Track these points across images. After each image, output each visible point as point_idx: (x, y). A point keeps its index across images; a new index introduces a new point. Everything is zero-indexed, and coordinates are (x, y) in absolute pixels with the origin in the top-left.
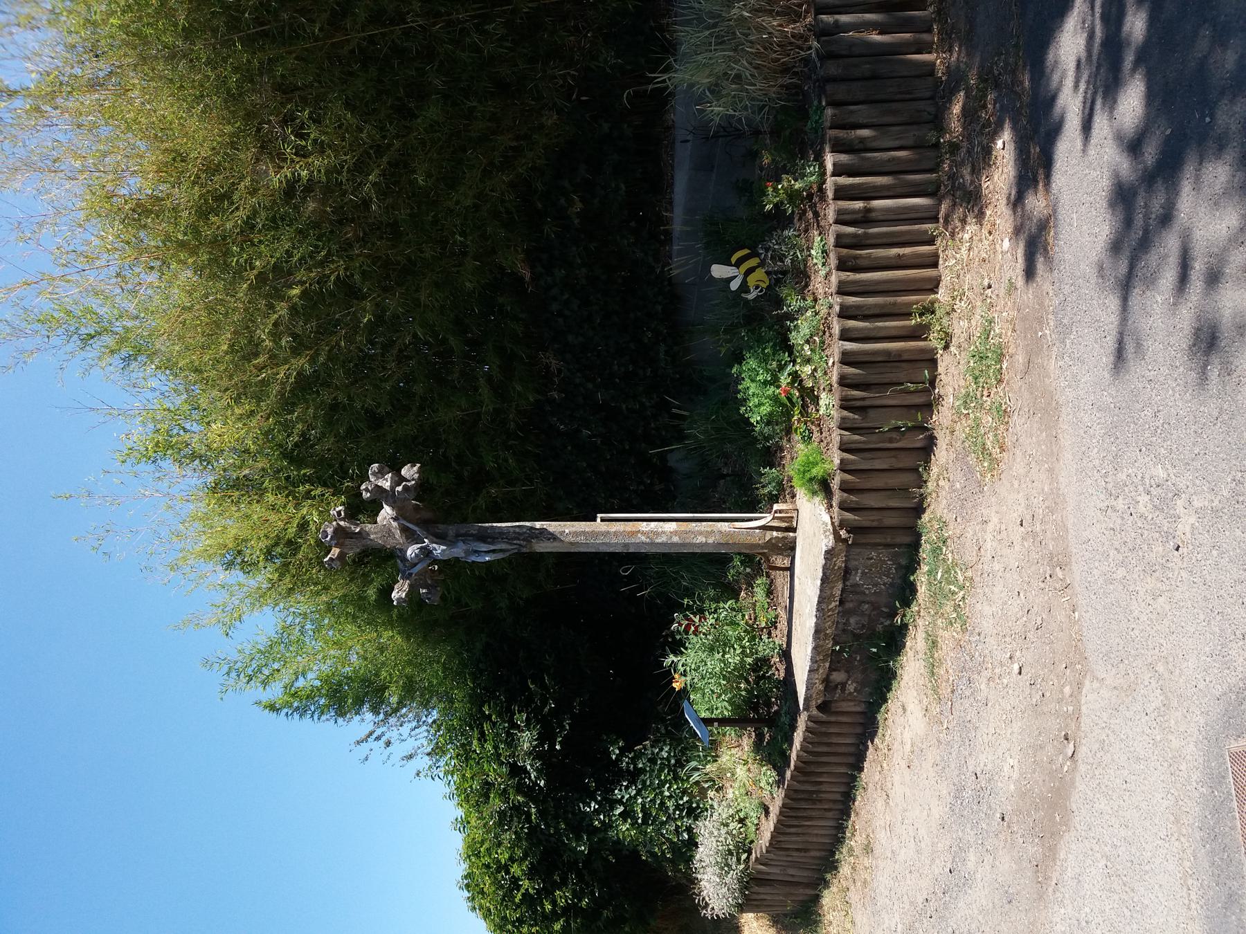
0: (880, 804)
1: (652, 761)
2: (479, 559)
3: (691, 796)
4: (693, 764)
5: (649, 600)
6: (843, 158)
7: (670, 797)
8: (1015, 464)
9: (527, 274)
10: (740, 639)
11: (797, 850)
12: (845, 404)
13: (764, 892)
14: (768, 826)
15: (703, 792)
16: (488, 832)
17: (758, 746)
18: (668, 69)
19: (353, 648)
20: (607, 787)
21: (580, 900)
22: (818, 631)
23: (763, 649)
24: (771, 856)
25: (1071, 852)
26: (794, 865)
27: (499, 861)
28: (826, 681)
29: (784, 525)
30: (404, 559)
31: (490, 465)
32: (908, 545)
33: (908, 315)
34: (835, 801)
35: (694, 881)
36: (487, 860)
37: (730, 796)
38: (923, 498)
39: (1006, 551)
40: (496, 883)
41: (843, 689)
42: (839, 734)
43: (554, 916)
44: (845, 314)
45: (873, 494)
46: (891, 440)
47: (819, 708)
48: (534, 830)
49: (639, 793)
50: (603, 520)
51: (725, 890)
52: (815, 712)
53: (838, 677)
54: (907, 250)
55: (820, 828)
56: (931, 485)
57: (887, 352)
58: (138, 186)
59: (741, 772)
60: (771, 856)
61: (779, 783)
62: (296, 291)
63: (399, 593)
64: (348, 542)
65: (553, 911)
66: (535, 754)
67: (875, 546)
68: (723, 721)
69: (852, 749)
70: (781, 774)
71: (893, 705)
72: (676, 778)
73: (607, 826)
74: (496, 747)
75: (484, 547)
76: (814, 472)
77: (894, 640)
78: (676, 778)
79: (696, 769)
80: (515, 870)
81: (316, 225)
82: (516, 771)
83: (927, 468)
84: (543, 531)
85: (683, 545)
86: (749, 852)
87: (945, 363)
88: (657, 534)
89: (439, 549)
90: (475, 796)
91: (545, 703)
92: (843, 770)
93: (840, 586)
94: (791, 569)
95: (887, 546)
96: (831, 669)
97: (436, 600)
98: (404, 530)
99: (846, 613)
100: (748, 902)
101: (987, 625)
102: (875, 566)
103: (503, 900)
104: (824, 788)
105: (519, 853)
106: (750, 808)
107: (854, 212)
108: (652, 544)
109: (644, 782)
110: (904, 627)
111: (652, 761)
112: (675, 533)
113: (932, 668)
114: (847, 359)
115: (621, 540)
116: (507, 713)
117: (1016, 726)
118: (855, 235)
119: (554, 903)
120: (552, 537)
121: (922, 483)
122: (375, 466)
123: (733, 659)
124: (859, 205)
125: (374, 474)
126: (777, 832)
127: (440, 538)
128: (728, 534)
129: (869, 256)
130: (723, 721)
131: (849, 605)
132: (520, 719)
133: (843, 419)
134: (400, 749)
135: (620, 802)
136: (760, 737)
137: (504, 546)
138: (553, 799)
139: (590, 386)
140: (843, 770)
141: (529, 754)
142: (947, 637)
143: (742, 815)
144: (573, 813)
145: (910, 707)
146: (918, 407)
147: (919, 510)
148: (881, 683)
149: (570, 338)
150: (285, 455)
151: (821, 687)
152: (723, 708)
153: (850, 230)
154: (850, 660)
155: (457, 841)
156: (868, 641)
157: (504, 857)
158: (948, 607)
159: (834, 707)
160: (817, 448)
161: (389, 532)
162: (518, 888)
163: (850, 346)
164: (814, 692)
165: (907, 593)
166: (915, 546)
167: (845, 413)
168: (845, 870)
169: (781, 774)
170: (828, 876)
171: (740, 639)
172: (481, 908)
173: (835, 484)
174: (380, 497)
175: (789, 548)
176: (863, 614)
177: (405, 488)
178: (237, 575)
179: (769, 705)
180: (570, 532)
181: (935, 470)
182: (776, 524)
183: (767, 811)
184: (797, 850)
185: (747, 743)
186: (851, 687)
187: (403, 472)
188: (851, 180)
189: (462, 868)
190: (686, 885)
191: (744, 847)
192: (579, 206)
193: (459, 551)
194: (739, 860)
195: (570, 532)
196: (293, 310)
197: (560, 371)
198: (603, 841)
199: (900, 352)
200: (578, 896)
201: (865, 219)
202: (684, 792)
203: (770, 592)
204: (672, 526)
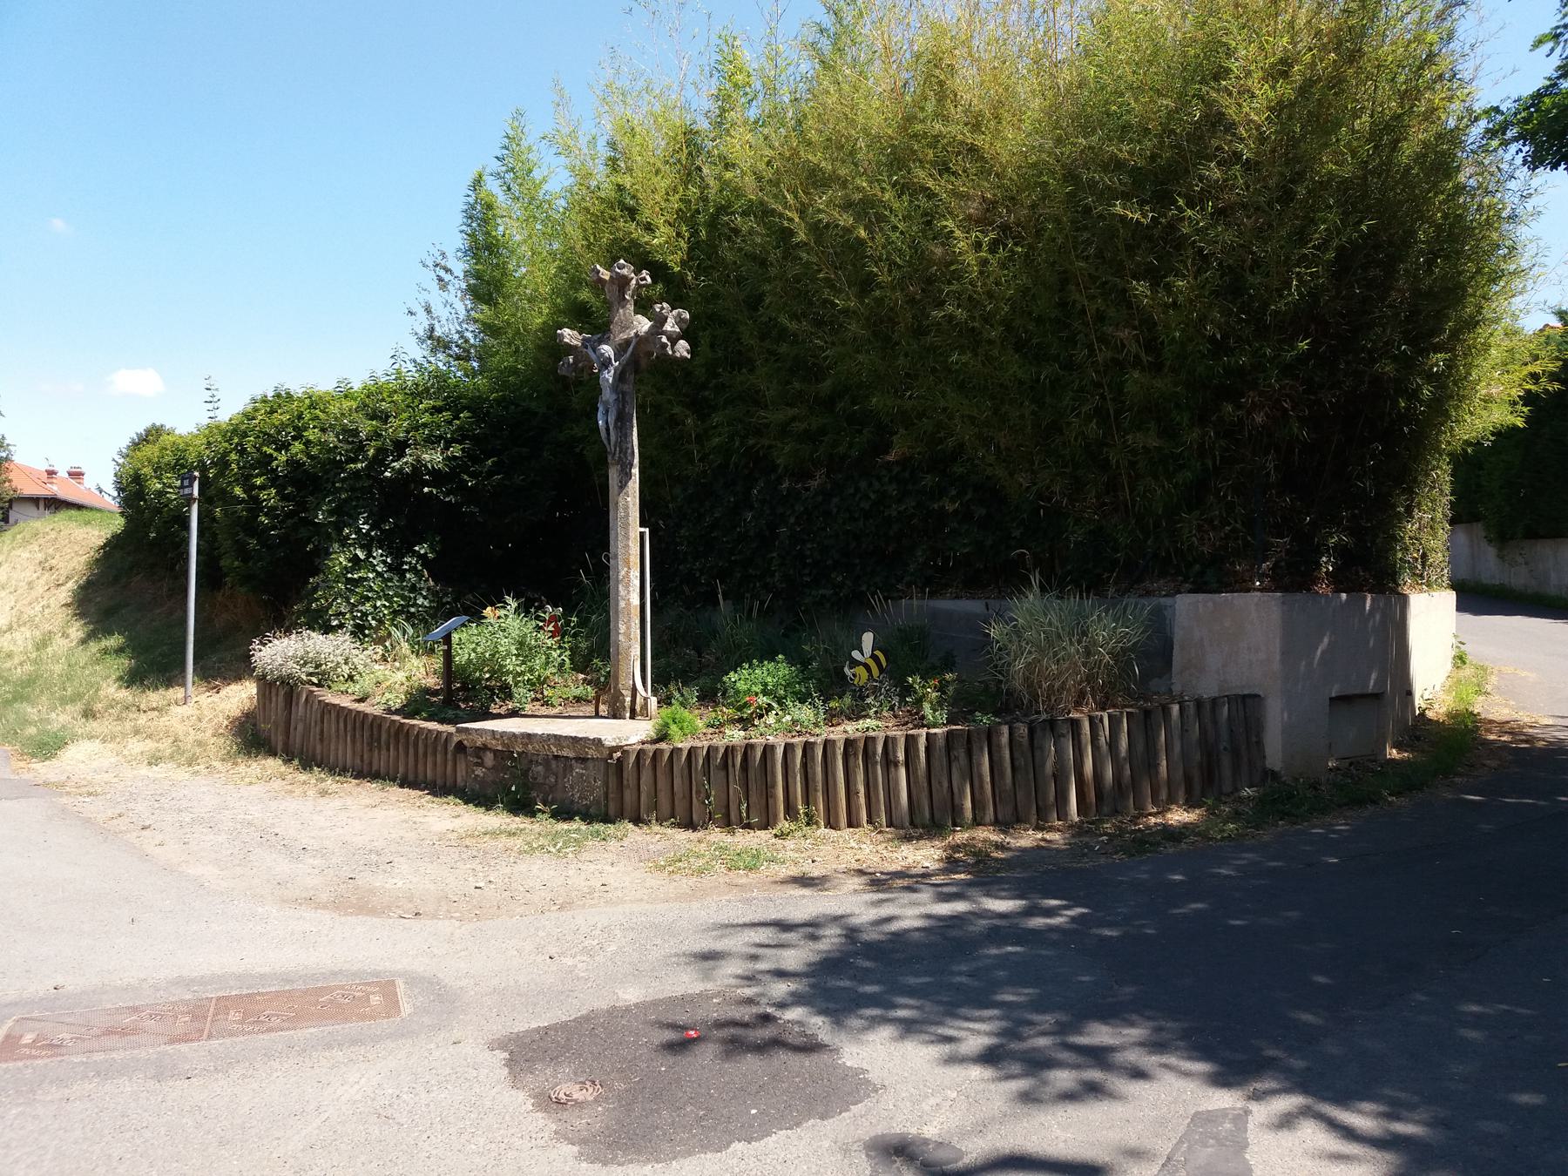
0: (368, 801)
1: (413, 589)
2: (600, 415)
3: (377, 629)
4: (410, 631)
5: (566, 579)
6: (941, 742)
7: (375, 607)
8: (656, 881)
9: (891, 458)
10: (531, 670)
11: (322, 731)
12: (730, 750)
13: (279, 700)
14: (345, 702)
15: (381, 641)
16: (336, 419)
17: (427, 691)
18: (1043, 589)
19: (533, 273)
20: (385, 541)
21: (266, 515)
22: (529, 736)
23: (520, 692)
24: (316, 706)
25: (325, 916)
26: (307, 729)
27: (306, 429)
28: (485, 748)
29: (638, 708)
30: (601, 342)
31: (716, 419)
32: (607, 814)
33: (807, 803)
34: (371, 764)
35: (288, 632)
36: (307, 416)
37: (377, 667)
38: (647, 823)
39: (583, 876)
40: (283, 426)
41: (477, 764)
42: (435, 764)
43: (249, 488)
44: (808, 747)
45: (651, 781)
46: (698, 792)
47: (460, 743)
48: (340, 466)
49: (379, 574)
50: (642, 535)
51: (280, 661)
52: (456, 739)
53: (489, 759)
54: (862, 800)
55: (344, 752)
56: (656, 828)
57: (774, 785)
58: (968, 83)
59: (400, 676)
60: (316, 706)
61: (389, 711)
62: (863, 233)
63: (569, 335)
64: (615, 288)
65: (254, 487)
66: (418, 467)
67: (606, 784)
68: (448, 656)
69: (421, 777)
70: (397, 712)
71: (462, 808)
72: (395, 613)
73: (344, 542)
74: (425, 425)
75: (611, 419)
76: (674, 728)
77: (521, 806)
78: (395, 613)
79: (404, 632)
80: (297, 447)
81: (922, 257)
82: (400, 447)
83: (673, 825)
84: (629, 475)
85: (617, 612)
86: (319, 685)
87: (763, 835)
88: (627, 586)
89: (609, 376)
90: (373, 404)
91: (473, 475)
92: (401, 770)
93: (571, 755)
94: (597, 716)
95: (606, 794)
96: (496, 752)
97: (562, 372)
98: (628, 342)
99: (546, 762)
100: (267, 686)
101: (522, 867)
102: (587, 784)
103: (265, 434)
104: (384, 752)
105: (314, 451)
106: (365, 684)
107: (895, 752)
108: (618, 582)
109: (390, 580)
110: (532, 814)
111: (413, 589)
112: (628, 604)
113: (494, 834)
114: (768, 750)
115: (621, 551)
116: (461, 436)
117: (432, 887)
118: (875, 753)
119: (263, 487)
120: (623, 486)
121: (660, 821)
122: (687, 315)
123: (511, 664)
124: (901, 756)
125: (679, 314)
126: (339, 710)
127: (620, 377)
128: (628, 655)
129: (857, 766)
130: (448, 656)
131: (554, 764)
132: (456, 450)
133: (717, 749)
134: (436, 298)
135: (369, 555)
136: (435, 693)
137: (613, 438)
138: (371, 486)
139: (792, 520)
140: (401, 770)
141: (418, 460)
142: (518, 842)
143: (357, 677)
144: (356, 507)
145: (457, 821)
146: (727, 815)
147: (637, 821)
148: (481, 798)
149: (835, 500)
150: (722, 209)
151: (479, 744)
152: (461, 657)
153: (880, 750)
154: (506, 769)
155: (325, 384)
156: (525, 785)
157: (312, 434)
158: (542, 841)
159: (460, 757)
160: (698, 729)
161: (625, 328)
162: (278, 450)
163: (780, 752)
164: (475, 736)
165: (563, 813)
166: (607, 819)
167: (722, 751)
168: (303, 777)
169: (397, 712)
170: (296, 762)
171: (531, 670)
172: (256, 410)
173: (663, 746)
174: (660, 321)
175: (615, 714)
176: (546, 778)
177: (665, 346)
178: (604, 152)
179: (465, 700)
180: (628, 502)
181: (669, 831)
182: (639, 700)
183: (361, 700)
184: (322, 731)
185: (432, 682)
186: (479, 772)
187: (682, 342)
188: (922, 749)
189: (297, 390)
190: (282, 623)
191: (324, 680)
192: (950, 508)
193: (607, 395)
194: (311, 674)
195: (628, 502)
196: (847, 230)
197: (807, 489)
198: (329, 538)
199: (774, 797)
200: (271, 512)
201: (889, 762)
202: (381, 622)
203: (578, 699)
204: (636, 601)
